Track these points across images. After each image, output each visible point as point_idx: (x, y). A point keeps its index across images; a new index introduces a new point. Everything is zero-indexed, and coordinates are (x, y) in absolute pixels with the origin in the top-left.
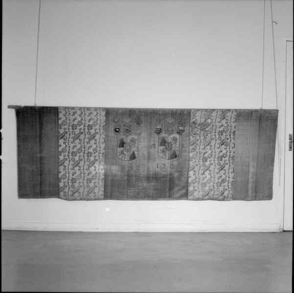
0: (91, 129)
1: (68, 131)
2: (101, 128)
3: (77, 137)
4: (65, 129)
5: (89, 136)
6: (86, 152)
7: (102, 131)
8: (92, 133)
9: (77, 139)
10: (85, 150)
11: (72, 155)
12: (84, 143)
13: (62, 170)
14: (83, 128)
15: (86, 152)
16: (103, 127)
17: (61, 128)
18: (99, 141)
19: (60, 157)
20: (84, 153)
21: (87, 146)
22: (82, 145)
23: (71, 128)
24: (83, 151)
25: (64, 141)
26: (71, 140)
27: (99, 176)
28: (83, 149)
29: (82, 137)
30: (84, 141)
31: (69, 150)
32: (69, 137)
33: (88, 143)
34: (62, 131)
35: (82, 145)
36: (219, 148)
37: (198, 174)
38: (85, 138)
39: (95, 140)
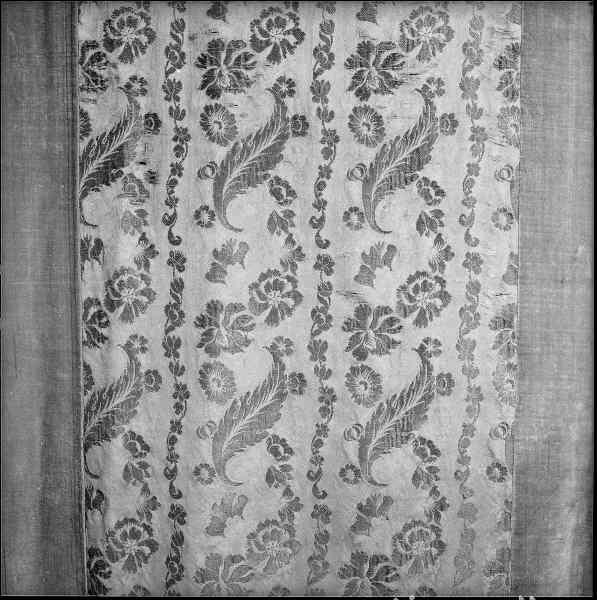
0: (390, 85)
1: (163, 109)
2: (487, 72)
3: (258, 163)
4: (134, 88)
5: (220, 153)
6: (342, 309)
7: (491, 100)
8: (395, 128)
9: (250, 179)
10: (324, 290)
11: (207, 343)
12: (170, 221)
13: (112, 481)
14: (304, 83)
15: (193, 307)
16: (500, 64)
17: (97, 83)
18: (468, 202)
19: (90, 356)
20: (321, 319)
21: (199, 246)
22: (304, 236)
23: (188, 75)
24: (311, 301)
25: (271, 205)
26: (344, 193)
27: (469, 536)
28: (307, 277)
29: (299, 160)
30: (320, 205)
31: (178, 286)
32: (177, 169)
33: (203, 217)
34: (101, 112)
35: (304, 236)
36: (355, 217)
37: (314, 476)
38: (325, 172)
39: (281, 191)
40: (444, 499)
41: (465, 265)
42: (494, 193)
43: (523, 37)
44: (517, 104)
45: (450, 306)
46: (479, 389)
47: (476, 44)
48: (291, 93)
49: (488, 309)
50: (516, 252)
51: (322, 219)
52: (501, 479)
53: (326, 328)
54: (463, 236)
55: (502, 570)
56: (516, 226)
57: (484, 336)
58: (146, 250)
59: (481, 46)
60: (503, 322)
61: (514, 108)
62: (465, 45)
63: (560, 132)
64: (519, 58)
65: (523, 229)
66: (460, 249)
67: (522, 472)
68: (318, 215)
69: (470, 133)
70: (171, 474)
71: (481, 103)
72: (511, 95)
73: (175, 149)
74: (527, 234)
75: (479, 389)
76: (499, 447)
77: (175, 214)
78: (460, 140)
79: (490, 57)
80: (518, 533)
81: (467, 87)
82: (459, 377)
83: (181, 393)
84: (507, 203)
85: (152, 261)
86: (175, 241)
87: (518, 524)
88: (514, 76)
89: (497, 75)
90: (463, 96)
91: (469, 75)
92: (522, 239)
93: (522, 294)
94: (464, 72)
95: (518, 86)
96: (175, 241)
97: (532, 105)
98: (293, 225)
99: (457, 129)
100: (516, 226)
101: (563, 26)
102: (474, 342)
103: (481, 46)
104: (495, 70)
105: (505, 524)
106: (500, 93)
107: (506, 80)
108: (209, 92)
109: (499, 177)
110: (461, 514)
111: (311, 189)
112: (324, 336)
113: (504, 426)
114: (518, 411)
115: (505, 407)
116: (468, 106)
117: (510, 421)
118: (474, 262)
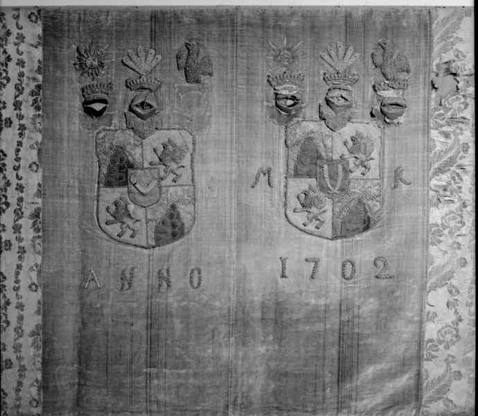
2: (26, 98)
7: (28, 111)
12: (16, 168)
16: (32, 94)
18: (18, 159)
24: (14, 206)
30: (18, 159)
40: (9, 300)
41: (17, 189)
42: (29, 155)
43: (43, 81)
44: (41, 112)
45: (9, 209)
46: (23, 248)
47: (21, 84)
48: (4, 107)
49: (28, 210)
50: (41, 182)
51: (19, 166)
52: (36, 291)
53: (21, 218)
54: (15, 175)
55: (38, 334)
56: (40, 170)
57: (26, 223)
58: (6, 183)
59: (23, 86)
60: (36, 215)
61: (39, 115)
62: (16, 85)
63: (60, 126)
64: (41, 91)
65: (44, 172)
66: (14, 181)
67: (45, 286)
68: (17, 164)
69: (18, 127)
70: (16, 289)
71: (23, 112)
72: (38, 108)
73: (19, 134)
74: (47, 174)
75: (23, 248)
76: (34, 275)
77: (20, 165)
78: (14, 129)
79: (27, 91)
80: (44, 316)
81: (17, 105)
82: (14, 242)
83: (22, 251)
84: (35, 159)
85: (8, 188)
86: (18, 178)
87: (44, 311)
88: (39, 99)
89: (31, 99)
90: (15, 109)
91: (17, 99)
92: (44, 177)
93: (43, 202)
94: (16, 97)
95: (41, 104)
96: (18, 178)
97: (47, 113)
98: (6, 170)
99: (13, 125)
100: (40, 170)
101: (61, 75)
102: (21, 225)
103: (23, 86)
104: (30, 97)
105: (38, 312)
106: (32, 108)
107: (35, 101)
108: (35, 108)
109: (32, 147)
110: (17, 307)
111: (13, 152)
112: (20, 222)
113: (36, 265)
114: (43, 258)
115: (37, 256)
116: (17, 114)
117: (39, 263)
118: (20, 188)
